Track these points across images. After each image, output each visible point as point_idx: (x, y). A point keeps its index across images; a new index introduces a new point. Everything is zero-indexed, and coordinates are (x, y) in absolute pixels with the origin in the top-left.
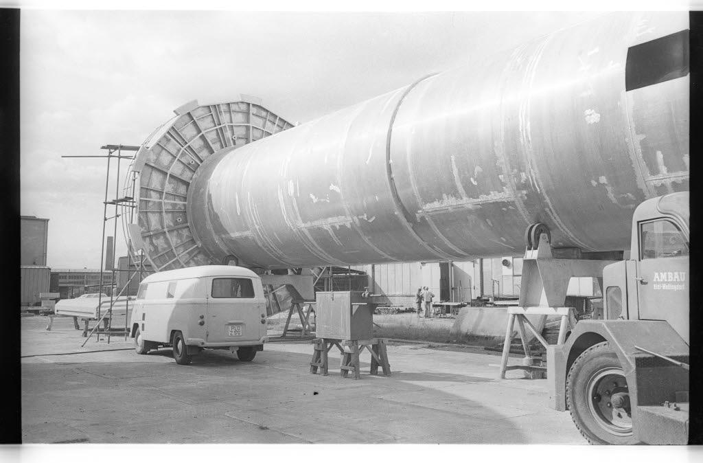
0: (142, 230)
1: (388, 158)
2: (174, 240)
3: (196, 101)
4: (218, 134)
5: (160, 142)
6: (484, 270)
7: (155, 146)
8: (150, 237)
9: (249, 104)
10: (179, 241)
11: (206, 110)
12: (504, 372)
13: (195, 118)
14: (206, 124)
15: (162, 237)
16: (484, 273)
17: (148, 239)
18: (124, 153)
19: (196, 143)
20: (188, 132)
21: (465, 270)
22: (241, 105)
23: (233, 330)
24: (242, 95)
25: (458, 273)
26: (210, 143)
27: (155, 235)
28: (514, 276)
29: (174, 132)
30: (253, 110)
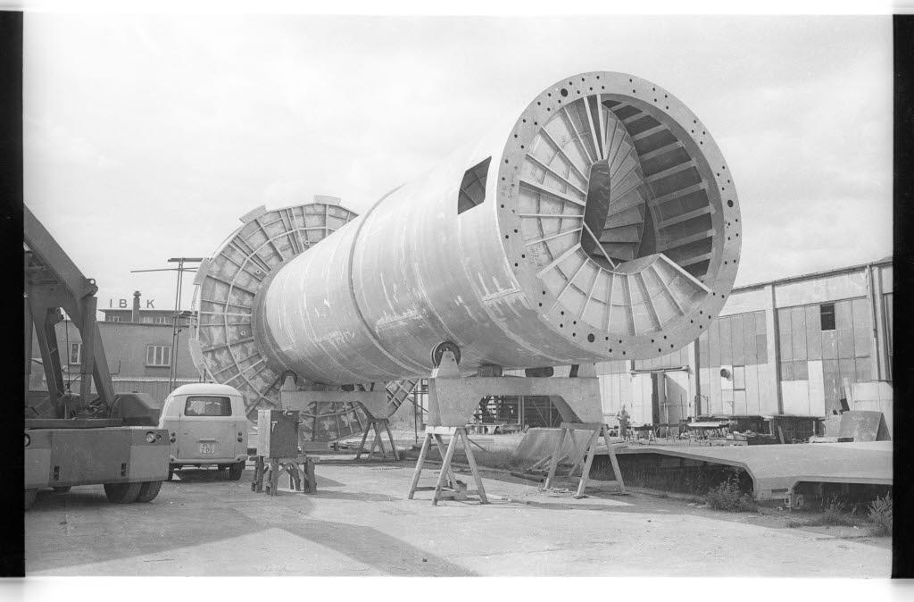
0: (204, 345)
1: (350, 274)
2: (237, 352)
3: (263, 207)
4: (289, 239)
5: (223, 252)
6: (701, 383)
7: (218, 257)
8: (212, 351)
9: (325, 205)
10: (244, 356)
11: (277, 215)
12: (413, 492)
13: (261, 225)
14: (275, 231)
15: (225, 352)
16: (702, 388)
17: (210, 355)
18: (186, 265)
19: (265, 252)
20: (257, 240)
21: (680, 383)
22: (316, 207)
23: (205, 448)
24: (316, 197)
25: (672, 387)
26: (279, 252)
27: (217, 349)
28: (734, 390)
29: (238, 241)
30: (330, 211)
